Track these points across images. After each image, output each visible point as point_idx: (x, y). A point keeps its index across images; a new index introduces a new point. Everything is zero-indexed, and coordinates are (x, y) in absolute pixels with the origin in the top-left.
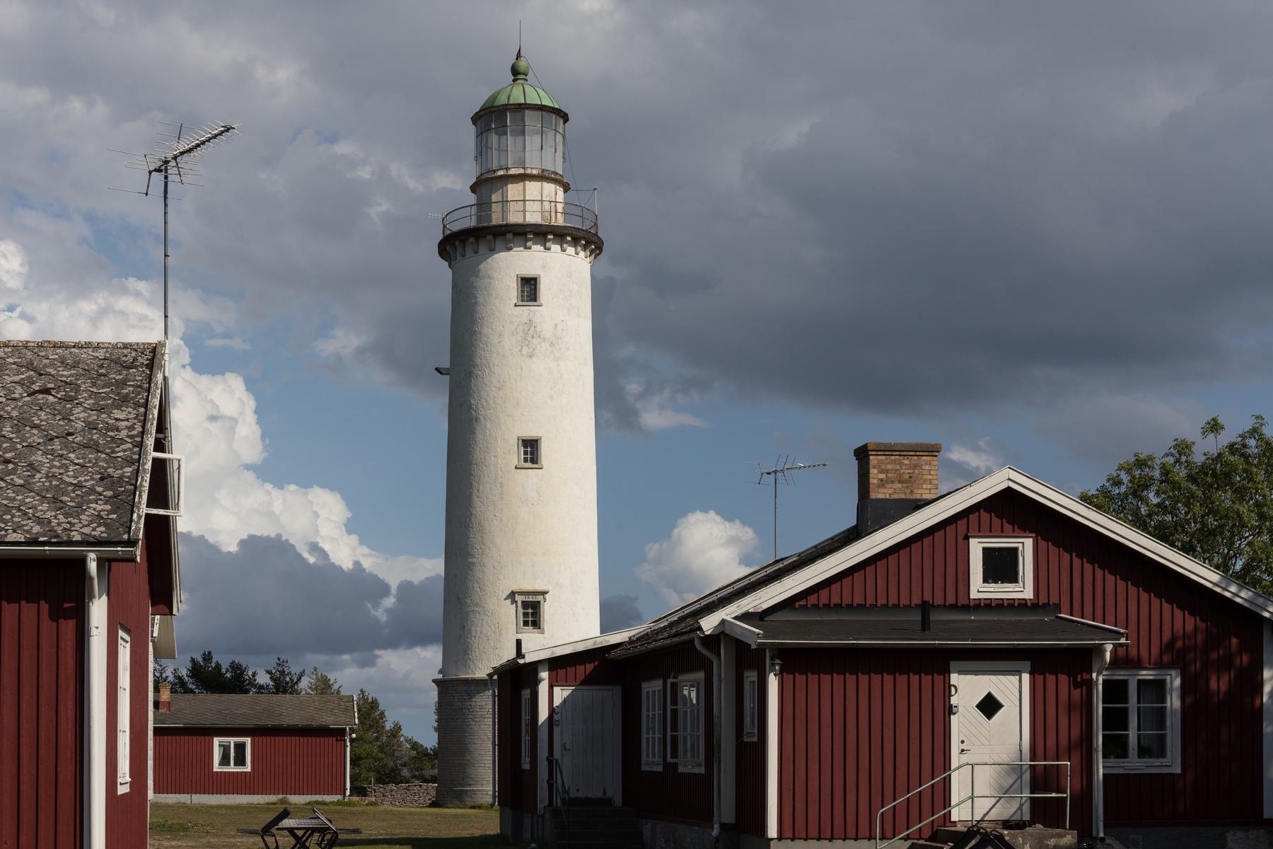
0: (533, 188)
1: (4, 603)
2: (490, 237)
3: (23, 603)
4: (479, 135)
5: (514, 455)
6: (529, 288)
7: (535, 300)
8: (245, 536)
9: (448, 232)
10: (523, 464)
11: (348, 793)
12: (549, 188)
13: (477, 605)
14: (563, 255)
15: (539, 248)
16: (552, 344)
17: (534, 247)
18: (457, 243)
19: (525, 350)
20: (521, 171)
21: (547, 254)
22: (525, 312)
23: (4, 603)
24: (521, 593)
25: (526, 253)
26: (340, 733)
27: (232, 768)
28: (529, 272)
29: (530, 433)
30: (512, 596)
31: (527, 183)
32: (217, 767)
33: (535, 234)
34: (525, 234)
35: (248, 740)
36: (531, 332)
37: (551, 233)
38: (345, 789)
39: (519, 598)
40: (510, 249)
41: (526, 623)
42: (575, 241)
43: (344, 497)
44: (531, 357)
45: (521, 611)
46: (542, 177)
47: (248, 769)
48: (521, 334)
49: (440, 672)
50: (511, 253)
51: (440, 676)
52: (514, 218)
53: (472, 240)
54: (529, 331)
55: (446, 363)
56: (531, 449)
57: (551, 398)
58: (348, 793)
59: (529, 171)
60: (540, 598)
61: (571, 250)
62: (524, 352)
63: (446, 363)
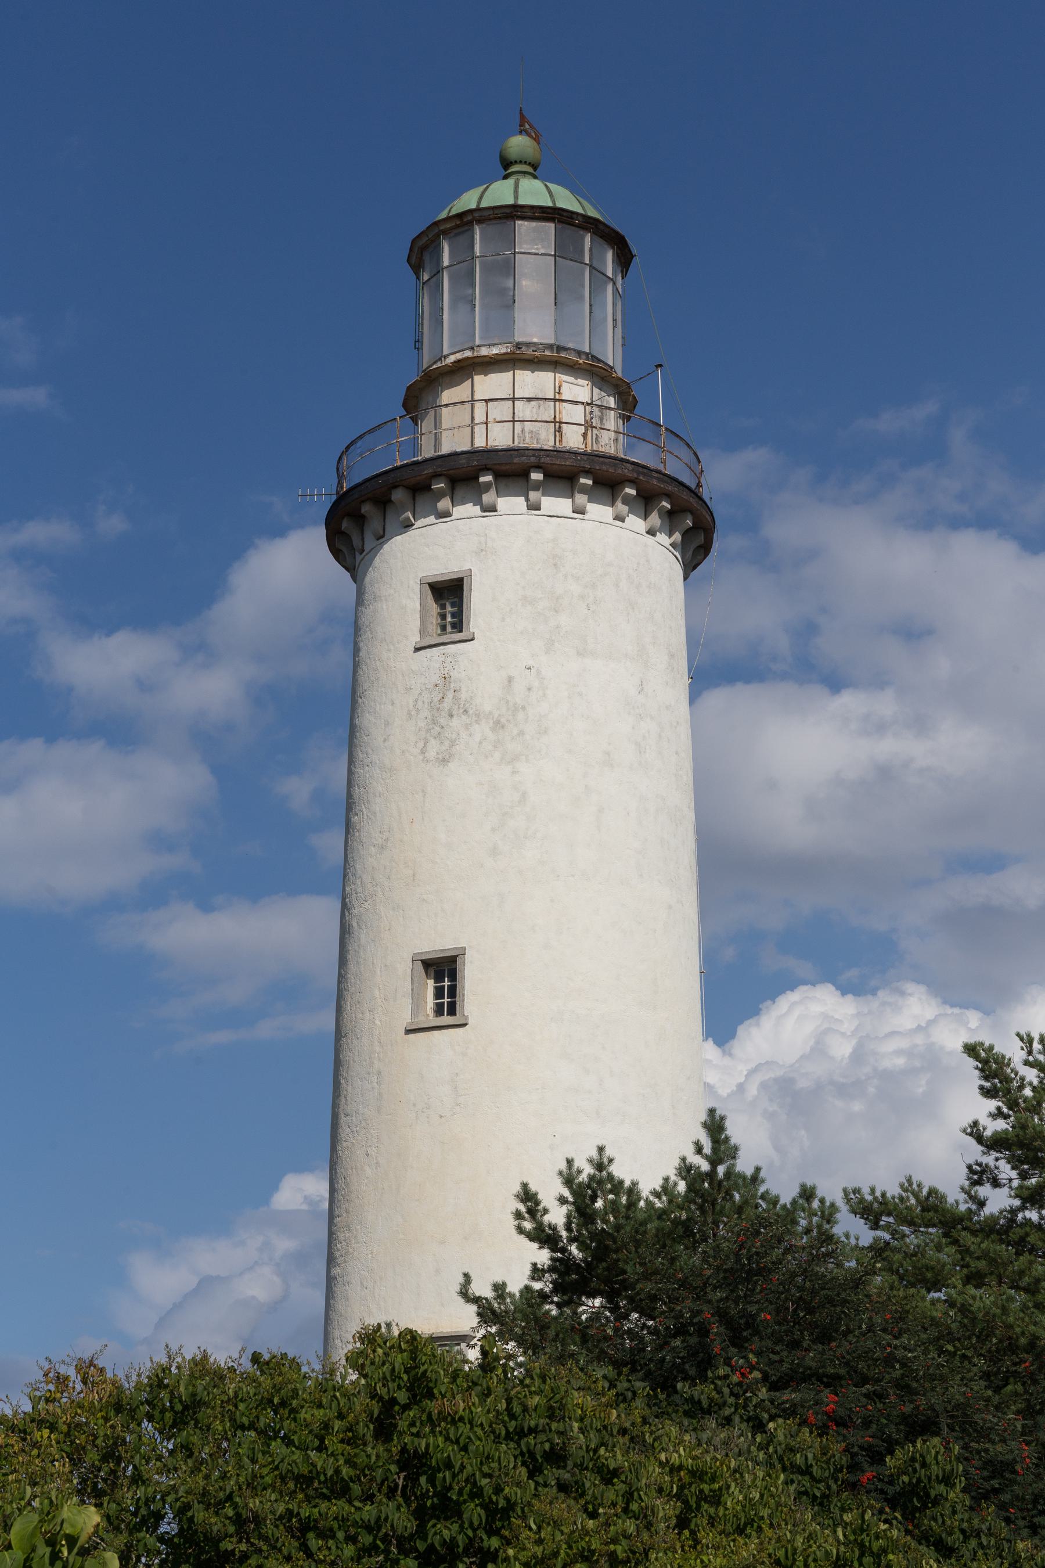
0: (489, 384)
8: (651, 1162)
10: (433, 1021)
12: (579, 389)
14: (534, 519)
15: (470, 509)
16: (498, 725)
17: (459, 511)
21: (491, 520)
25: (442, 528)
28: (443, 569)
29: (437, 944)
31: (477, 378)
36: (446, 705)
37: (485, 469)
40: (408, 526)
42: (645, 502)
44: (444, 761)
46: (519, 359)
50: (412, 533)
54: (446, 700)
57: (494, 852)
61: (561, 505)
62: (431, 754)
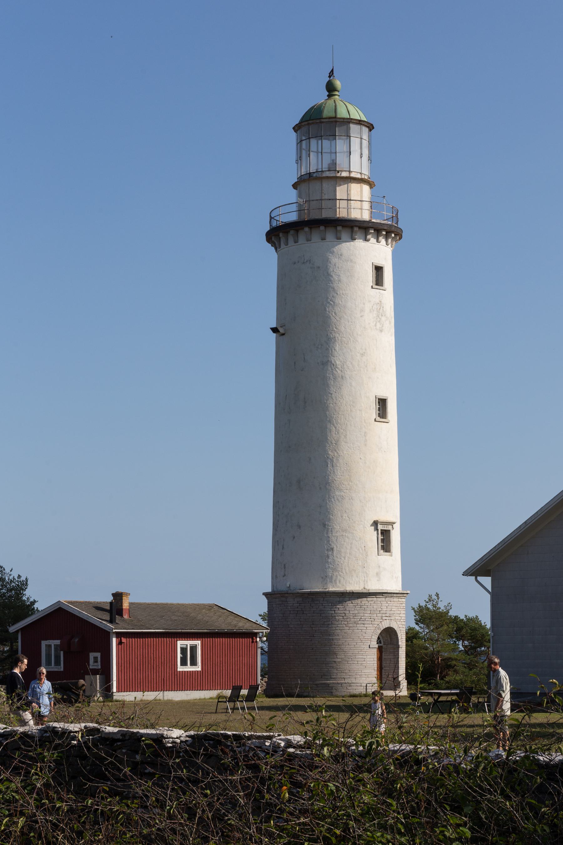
0: (355, 187)
1: (486, 620)
2: (306, 229)
4: (300, 142)
7: (382, 285)
9: (274, 224)
13: (345, 531)
18: (281, 235)
19: (378, 325)
23: (486, 620)
26: (252, 635)
27: (189, 668)
30: (375, 524)
32: (180, 669)
33: (360, 228)
34: (352, 227)
39: (380, 527)
45: (380, 537)
47: (198, 668)
48: (375, 312)
52: (342, 213)
53: (292, 232)
59: (353, 175)
60: (390, 528)
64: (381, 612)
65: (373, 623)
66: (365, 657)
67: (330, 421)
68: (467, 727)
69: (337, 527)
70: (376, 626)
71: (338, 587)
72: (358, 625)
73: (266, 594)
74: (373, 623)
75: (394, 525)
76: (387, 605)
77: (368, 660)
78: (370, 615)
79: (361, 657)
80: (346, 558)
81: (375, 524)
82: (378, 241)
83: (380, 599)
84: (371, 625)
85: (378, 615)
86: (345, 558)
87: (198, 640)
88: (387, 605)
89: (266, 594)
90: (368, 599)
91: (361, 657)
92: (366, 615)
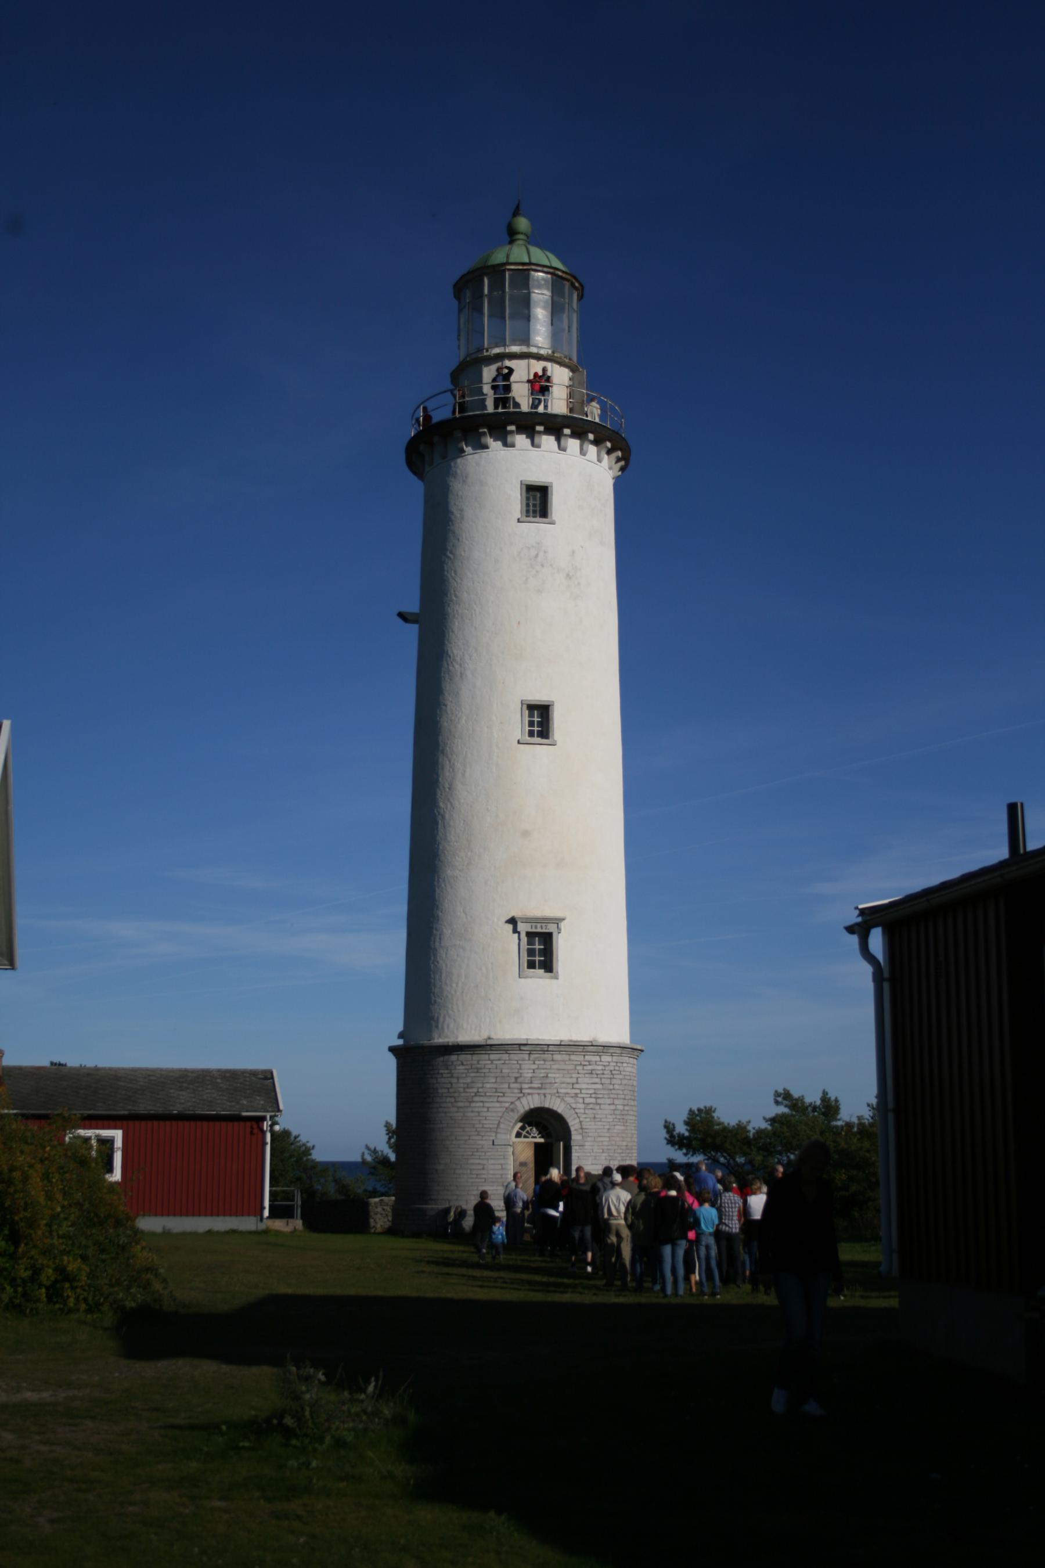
3: (338, 1103)
5: (516, 724)
6: (538, 500)
11: (266, 1213)
16: (568, 576)
18: (436, 439)
20: (524, 349)
22: (536, 528)
24: (527, 920)
28: (537, 478)
29: (539, 697)
30: (513, 921)
35: (117, 1135)
38: (263, 1208)
39: (522, 927)
41: (531, 965)
43: (398, 1064)
44: (539, 591)
49: (401, 1036)
51: (401, 1042)
55: (413, 606)
56: (540, 719)
58: (266, 1213)
60: (551, 928)
61: (592, 450)
63: (413, 606)
64: (520, 1080)
65: (500, 1099)
66: (485, 1162)
67: (443, 752)
68: (473, 1277)
69: (447, 932)
70: (507, 1105)
71: (446, 1037)
72: (473, 1105)
73: (392, 1049)
74: (500, 1099)
75: (562, 925)
76: (535, 1067)
77: (492, 1167)
78: (495, 1086)
79: (477, 1161)
80: (460, 985)
81: (513, 921)
82: (562, 448)
83: (516, 1057)
84: (498, 1105)
85: (512, 1085)
86: (457, 984)
87: (116, 1128)
88: (535, 1067)
89: (392, 1049)
90: (492, 1057)
91: (477, 1161)
92: (488, 1085)
